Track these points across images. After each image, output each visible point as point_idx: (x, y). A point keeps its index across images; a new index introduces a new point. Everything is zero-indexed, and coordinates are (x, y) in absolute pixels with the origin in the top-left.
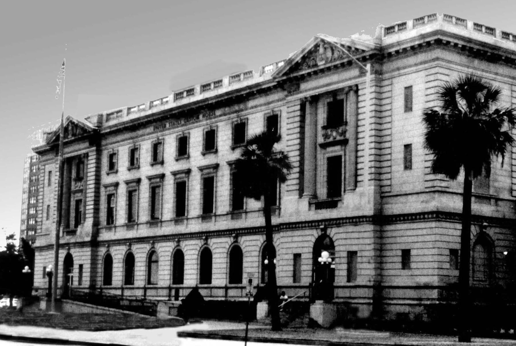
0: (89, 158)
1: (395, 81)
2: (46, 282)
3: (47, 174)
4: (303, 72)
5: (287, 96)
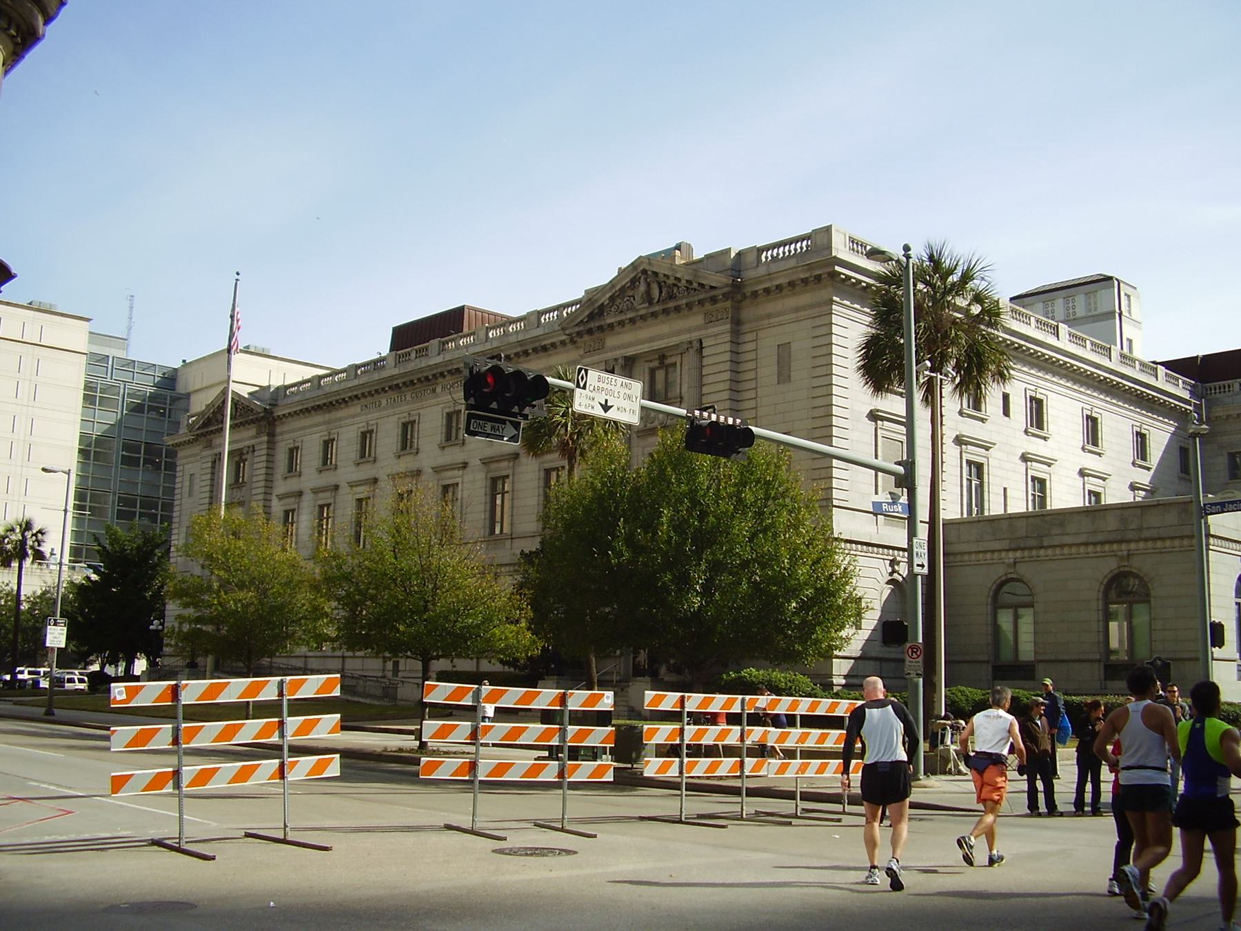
0: (256, 453)
1: (761, 334)
2: (382, 559)
3: (187, 478)
4: (609, 321)
5: (582, 357)
